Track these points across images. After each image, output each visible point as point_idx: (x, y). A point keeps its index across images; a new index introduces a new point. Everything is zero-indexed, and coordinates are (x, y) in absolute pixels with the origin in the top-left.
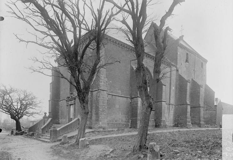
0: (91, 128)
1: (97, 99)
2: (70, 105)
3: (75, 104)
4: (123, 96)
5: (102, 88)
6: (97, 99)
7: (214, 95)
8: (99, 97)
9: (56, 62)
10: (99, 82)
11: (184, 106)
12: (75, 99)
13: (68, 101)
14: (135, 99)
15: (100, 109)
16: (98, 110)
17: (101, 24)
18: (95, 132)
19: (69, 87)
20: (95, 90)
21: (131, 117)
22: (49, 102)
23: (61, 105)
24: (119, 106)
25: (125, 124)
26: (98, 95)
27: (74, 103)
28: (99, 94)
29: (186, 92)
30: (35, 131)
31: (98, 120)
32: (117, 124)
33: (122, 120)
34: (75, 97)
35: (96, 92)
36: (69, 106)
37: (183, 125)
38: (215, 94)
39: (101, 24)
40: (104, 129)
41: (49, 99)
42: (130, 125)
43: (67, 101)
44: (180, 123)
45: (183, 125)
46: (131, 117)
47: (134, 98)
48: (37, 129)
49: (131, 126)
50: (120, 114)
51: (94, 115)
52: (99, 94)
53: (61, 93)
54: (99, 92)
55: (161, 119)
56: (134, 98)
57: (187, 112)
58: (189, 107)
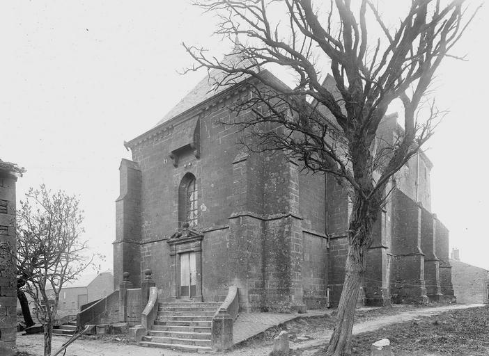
0: (265, 311)
1: (281, 240)
2: (180, 254)
3: (201, 251)
4: (316, 233)
5: (294, 212)
6: (281, 240)
7: (448, 236)
8: (289, 233)
9: (129, 149)
10: (286, 197)
11: (412, 257)
12: (201, 240)
13: (176, 245)
14: (339, 240)
15: (292, 264)
16: (288, 266)
17: (341, 74)
18: (301, 320)
19: (177, 211)
20: (274, 216)
21: (329, 283)
22: (115, 248)
23: (149, 253)
24: (310, 258)
25: (320, 299)
26: (286, 230)
27: (198, 248)
28: (290, 228)
29: (417, 227)
30: (96, 321)
31: (288, 290)
32: (308, 299)
33: (315, 289)
34: (202, 234)
35: (280, 221)
36: (178, 255)
37: (411, 298)
38: (450, 234)
39: (341, 74)
40: (300, 312)
41: (114, 239)
42: (328, 300)
43: (171, 245)
44: (405, 295)
45: (411, 298)
46: (329, 283)
47: (337, 238)
48: (101, 317)
49: (330, 303)
50: (312, 276)
51: (271, 277)
52: (290, 228)
53: (146, 223)
54: (289, 222)
55: (381, 286)
56: (337, 238)
57: (420, 270)
58: (422, 260)
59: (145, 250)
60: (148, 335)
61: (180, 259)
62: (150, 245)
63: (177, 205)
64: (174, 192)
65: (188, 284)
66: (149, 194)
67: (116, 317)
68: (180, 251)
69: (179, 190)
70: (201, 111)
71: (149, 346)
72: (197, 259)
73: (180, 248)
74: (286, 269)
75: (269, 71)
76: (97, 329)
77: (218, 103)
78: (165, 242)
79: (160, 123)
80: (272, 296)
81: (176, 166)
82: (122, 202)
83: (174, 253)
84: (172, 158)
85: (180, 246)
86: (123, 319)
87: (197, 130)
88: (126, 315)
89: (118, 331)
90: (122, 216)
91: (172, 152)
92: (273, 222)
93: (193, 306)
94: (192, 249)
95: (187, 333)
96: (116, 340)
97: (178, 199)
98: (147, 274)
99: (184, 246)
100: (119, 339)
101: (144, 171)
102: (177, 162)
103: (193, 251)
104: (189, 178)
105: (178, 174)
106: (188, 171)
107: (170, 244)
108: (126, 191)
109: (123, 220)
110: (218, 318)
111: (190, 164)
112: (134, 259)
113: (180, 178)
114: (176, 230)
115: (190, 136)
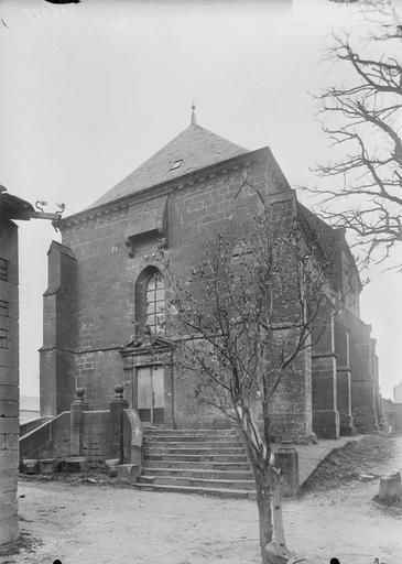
2: (138, 368)
14: (321, 359)
20: (281, 325)
41: (41, 345)
48: (44, 449)
59: (82, 361)
60: (143, 474)
61: (137, 375)
62: (91, 355)
63: (133, 305)
64: (127, 289)
65: (149, 406)
66: (88, 289)
67: (64, 449)
68: (139, 364)
69: (137, 285)
70: (171, 190)
71: (156, 490)
72: (165, 375)
73: (139, 360)
74: (300, 389)
75: (19, 234)
76: (42, 467)
77: (96, 216)
78: (117, 352)
79: (101, 203)
80: (279, 422)
81: (132, 256)
82: (54, 297)
83: (129, 366)
84: (128, 245)
85: (139, 358)
86: (77, 451)
87: (166, 214)
88: (81, 445)
89: (75, 468)
90: (54, 314)
91: (130, 238)
92: (279, 332)
93: (186, 435)
94: (159, 362)
95: (202, 471)
96: (87, 481)
97: (134, 297)
98: (117, 392)
99: (143, 357)
100: (93, 480)
101: (80, 259)
102: (133, 250)
103: (160, 365)
104: (151, 272)
105: (135, 267)
106: (149, 263)
107: (124, 354)
108: (58, 283)
109: (55, 321)
110: (283, 451)
111: (149, 254)
112: (69, 373)
113: (138, 273)
114: (132, 337)
115: (158, 218)
